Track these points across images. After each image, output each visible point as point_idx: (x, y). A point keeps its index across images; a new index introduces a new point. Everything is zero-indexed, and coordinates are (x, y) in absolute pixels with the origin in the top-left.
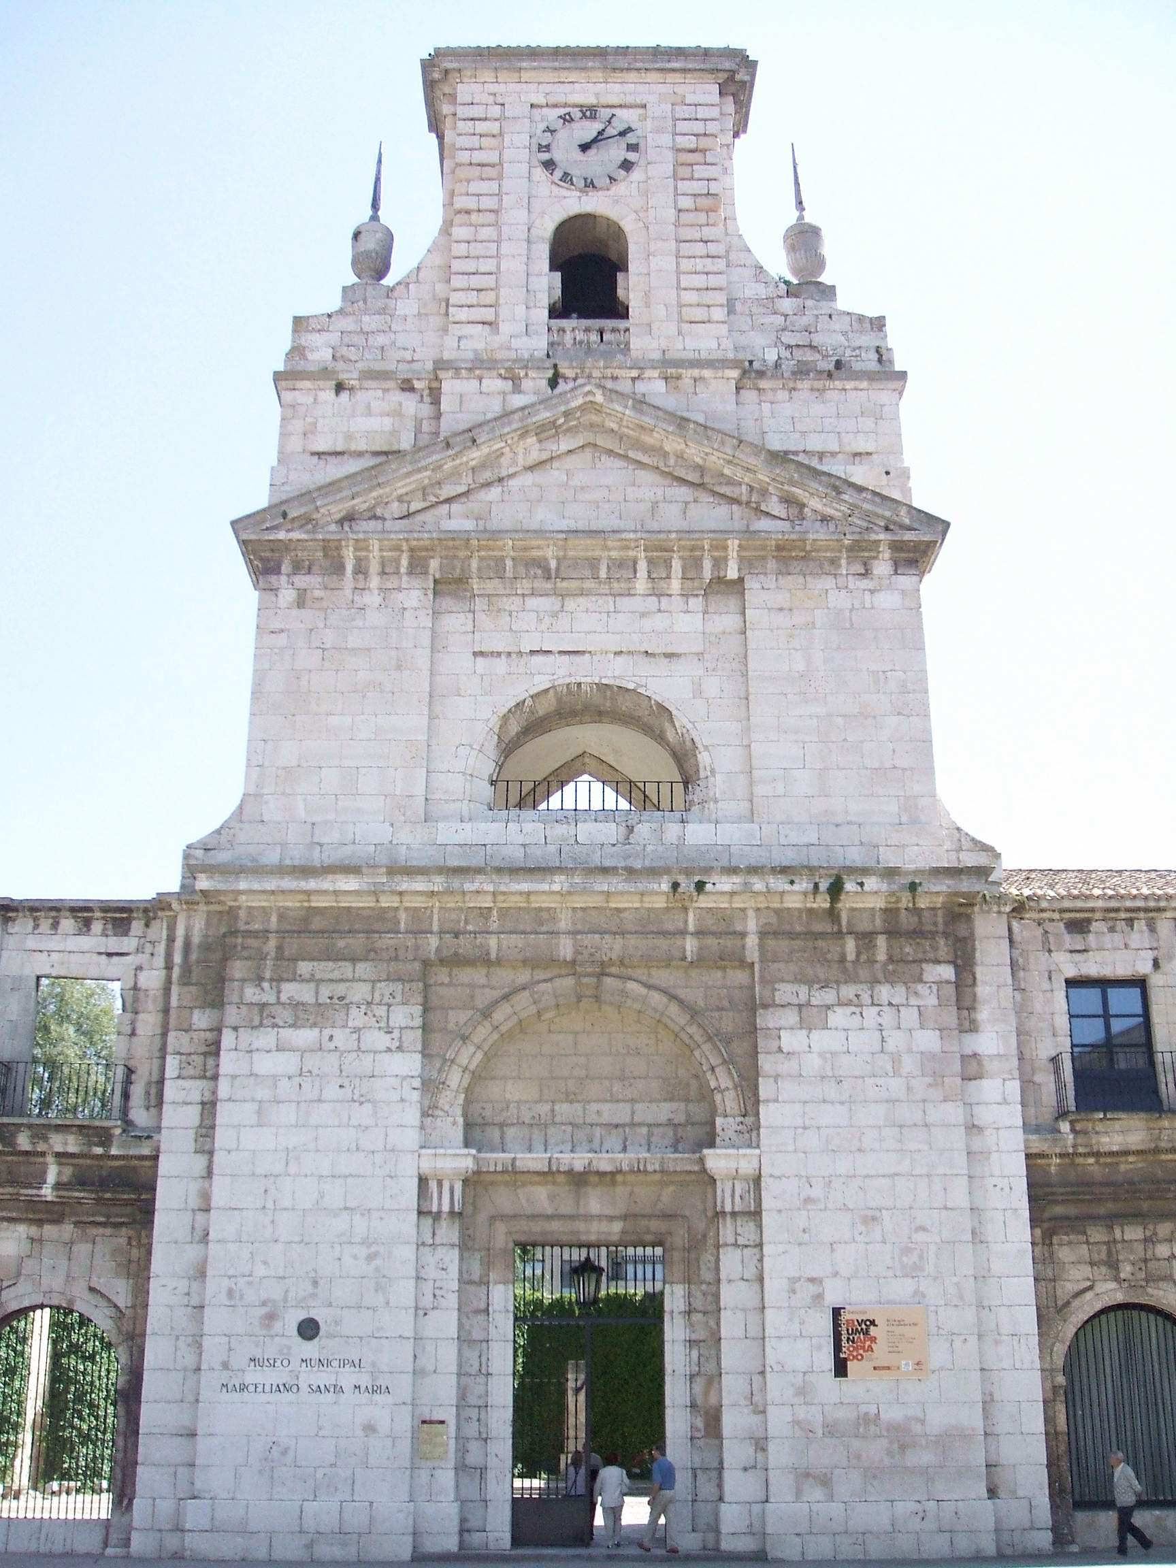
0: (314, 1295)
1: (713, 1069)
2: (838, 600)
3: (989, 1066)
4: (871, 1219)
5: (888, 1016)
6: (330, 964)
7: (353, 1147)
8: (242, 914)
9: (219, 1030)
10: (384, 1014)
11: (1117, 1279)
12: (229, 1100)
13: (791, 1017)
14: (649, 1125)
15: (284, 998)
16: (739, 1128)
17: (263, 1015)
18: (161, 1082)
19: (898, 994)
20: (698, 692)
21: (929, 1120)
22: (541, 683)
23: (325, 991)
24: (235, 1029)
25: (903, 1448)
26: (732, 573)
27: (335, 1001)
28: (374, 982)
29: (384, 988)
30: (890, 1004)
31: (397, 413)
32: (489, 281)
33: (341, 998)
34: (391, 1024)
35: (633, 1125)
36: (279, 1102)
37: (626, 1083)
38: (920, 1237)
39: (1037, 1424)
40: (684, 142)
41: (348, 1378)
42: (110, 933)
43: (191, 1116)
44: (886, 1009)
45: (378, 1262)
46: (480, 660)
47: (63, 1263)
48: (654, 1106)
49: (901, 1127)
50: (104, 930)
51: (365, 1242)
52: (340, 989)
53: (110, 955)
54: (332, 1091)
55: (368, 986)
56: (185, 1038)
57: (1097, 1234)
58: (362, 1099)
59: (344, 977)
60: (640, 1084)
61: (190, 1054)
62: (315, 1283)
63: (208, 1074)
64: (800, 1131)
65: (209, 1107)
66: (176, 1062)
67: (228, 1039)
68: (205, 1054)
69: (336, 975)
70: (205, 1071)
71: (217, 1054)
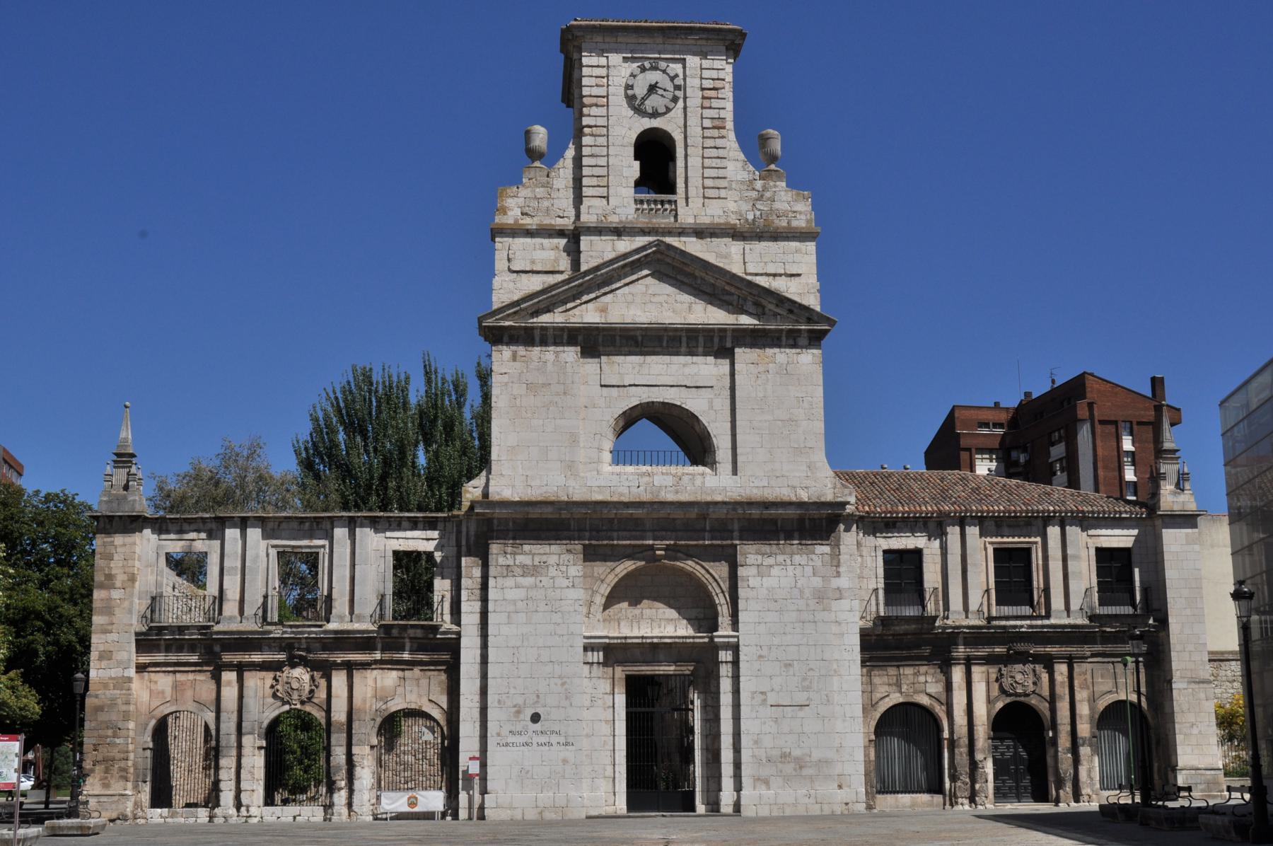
3: (845, 594)
4: (788, 665)
5: (799, 569)
8: (495, 522)
13: (753, 571)
20: (711, 407)
22: (635, 402)
23: (537, 559)
25: (801, 768)
26: (729, 345)
29: (566, 557)
32: (603, 172)
38: (811, 673)
39: (860, 756)
40: (707, 84)
41: (554, 739)
47: (415, 689)
51: (559, 677)
52: (544, 558)
54: (542, 607)
56: (470, 581)
57: (892, 671)
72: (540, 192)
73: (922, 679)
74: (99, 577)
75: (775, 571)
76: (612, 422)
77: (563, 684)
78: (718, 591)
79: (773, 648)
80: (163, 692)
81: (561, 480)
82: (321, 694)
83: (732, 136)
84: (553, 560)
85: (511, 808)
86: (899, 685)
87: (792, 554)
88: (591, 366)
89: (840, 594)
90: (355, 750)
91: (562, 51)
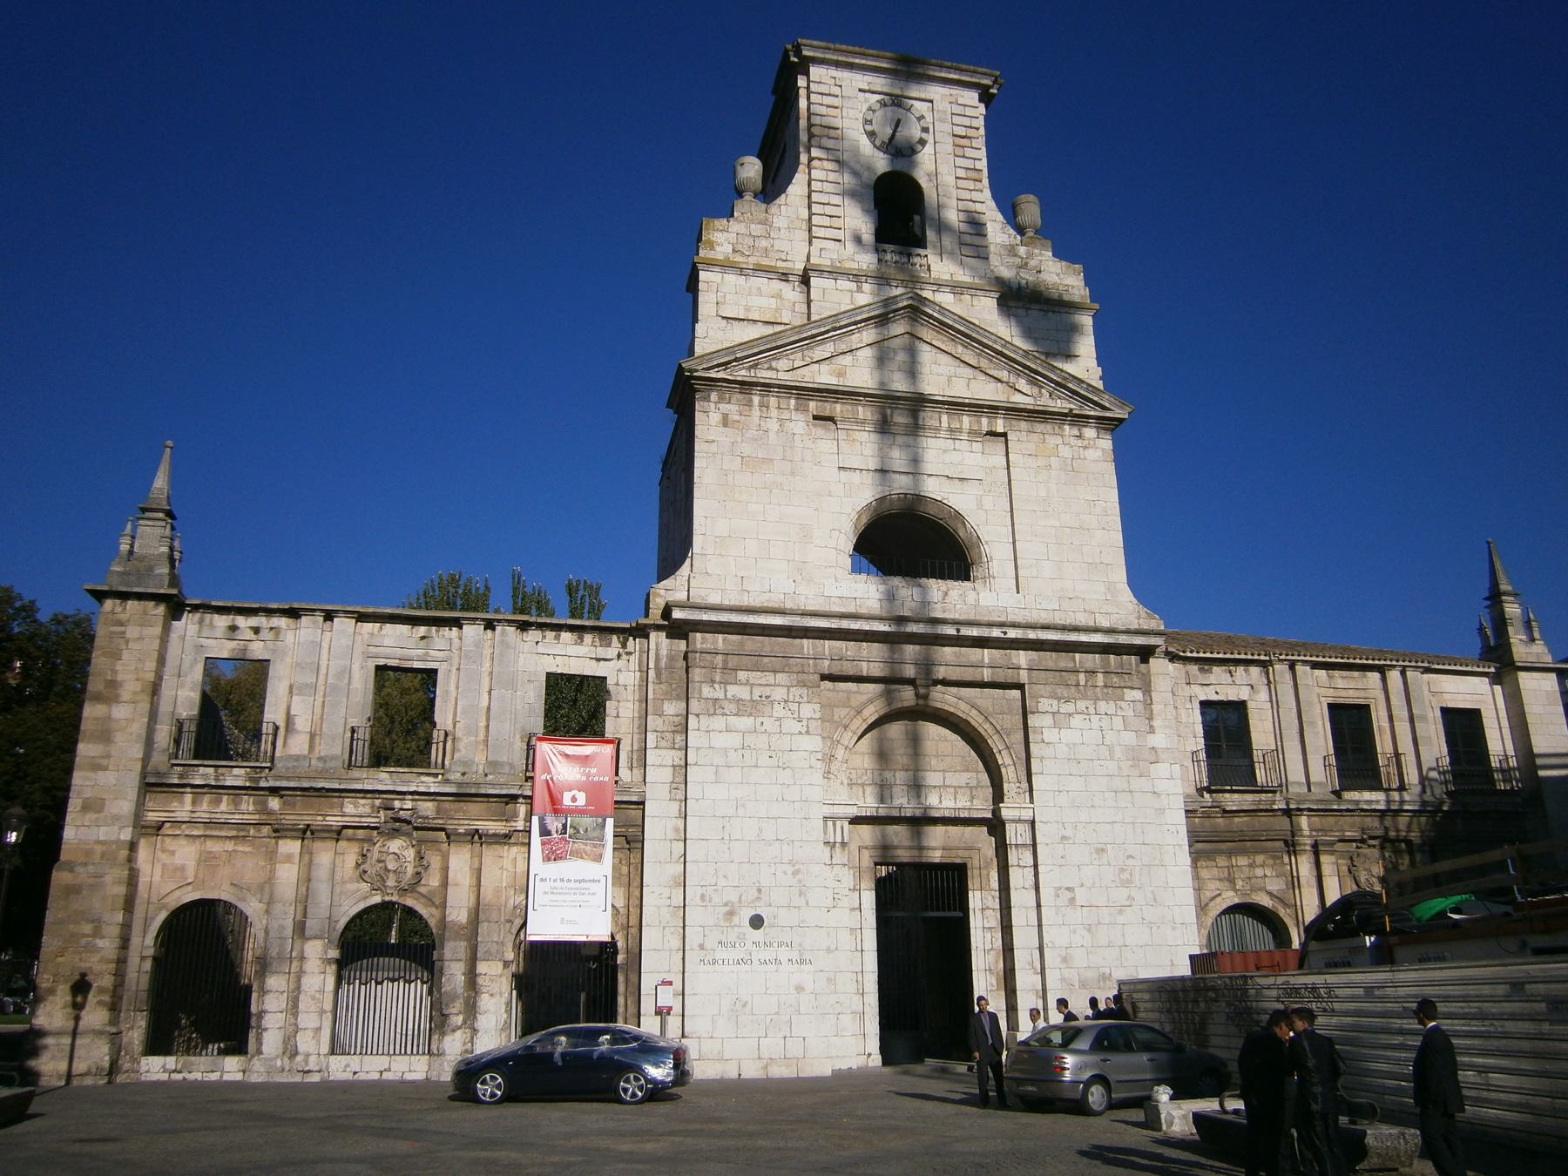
0: (758, 899)
2: (1065, 452)
3: (1163, 756)
5: (1106, 722)
11: (1236, 891)
13: (1047, 720)
17: (715, 707)
20: (980, 506)
23: (757, 692)
31: (779, 296)
35: (945, 786)
38: (1130, 862)
40: (960, 131)
45: (800, 876)
53: (598, 660)
54: (764, 760)
56: (659, 721)
57: (1222, 861)
60: (948, 759)
62: (759, 891)
67: (692, 721)
68: (674, 732)
69: (763, 681)
72: (757, 229)
73: (1259, 872)
74: (95, 685)
75: (1077, 721)
76: (854, 516)
77: (795, 873)
79: (1080, 826)
80: (182, 868)
81: (789, 587)
82: (433, 881)
83: (987, 193)
84: (779, 693)
85: (721, 1059)
86: (1231, 881)
89: (1155, 756)
90: (482, 967)
91: (774, 92)
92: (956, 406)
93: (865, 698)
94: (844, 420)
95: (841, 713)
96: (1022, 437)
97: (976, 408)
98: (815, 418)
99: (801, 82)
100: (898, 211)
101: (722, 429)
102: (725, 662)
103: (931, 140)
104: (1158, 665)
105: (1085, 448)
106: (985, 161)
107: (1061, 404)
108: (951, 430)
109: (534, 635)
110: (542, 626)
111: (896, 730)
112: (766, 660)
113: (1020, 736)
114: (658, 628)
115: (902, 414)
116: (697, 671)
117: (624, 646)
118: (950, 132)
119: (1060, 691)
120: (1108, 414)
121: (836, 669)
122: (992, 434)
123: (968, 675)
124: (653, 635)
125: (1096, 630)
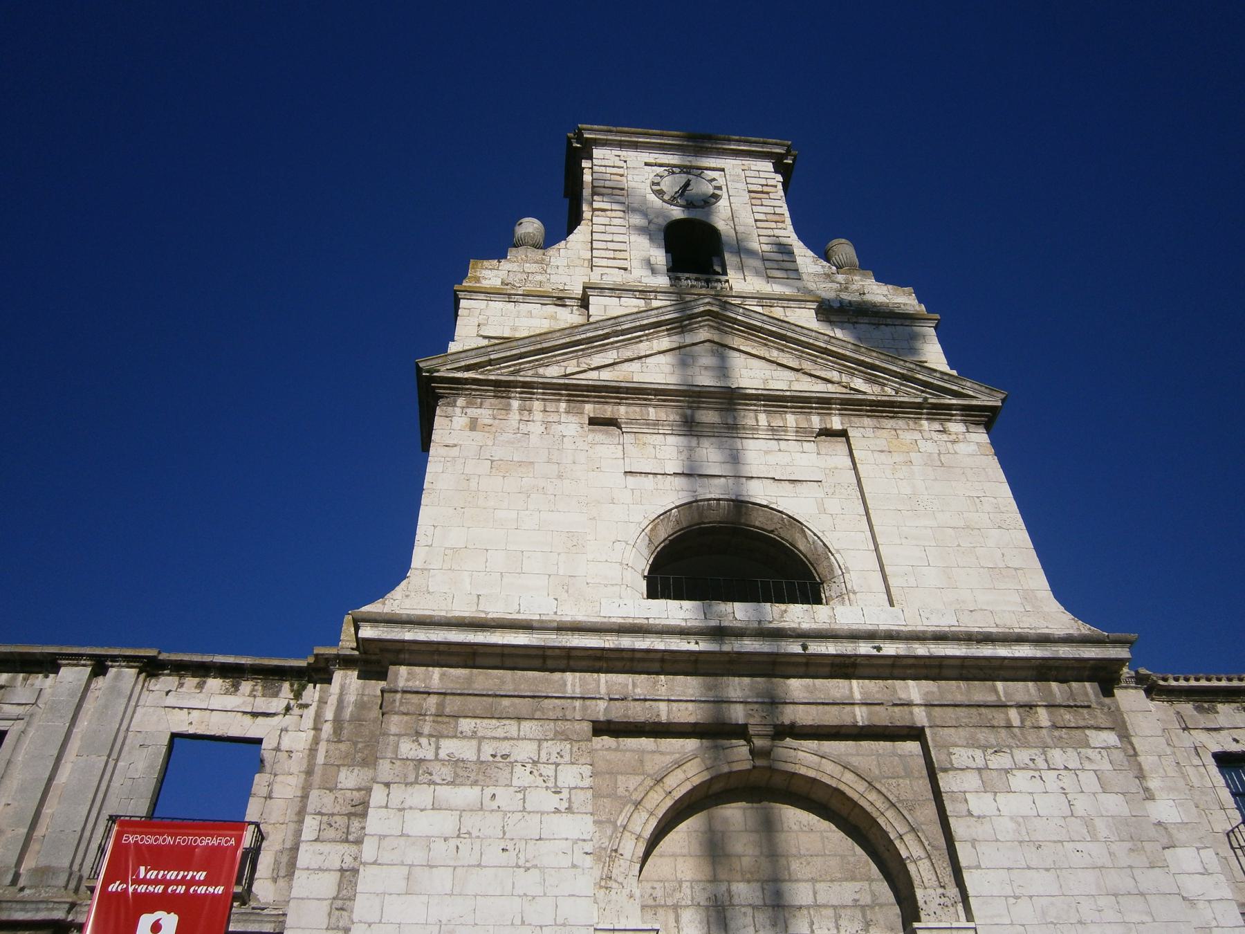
1: (901, 837)
3: (1181, 836)
5: (1068, 780)
6: (494, 721)
7: (518, 921)
9: (369, 790)
10: (551, 773)
12: (375, 863)
13: (970, 781)
14: (835, 907)
15: (443, 754)
16: (942, 900)
18: (295, 849)
19: (1070, 758)
21: (1143, 887)
23: (488, 749)
24: (387, 785)
27: (498, 759)
28: (540, 741)
29: (551, 748)
30: (1066, 768)
33: (504, 756)
34: (559, 784)
35: (817, 906)
36: (431, 867)
37: (803, 860)
42: (259, 694)
43: (327, 884)
44: (1063, 773)
46: (629, 478)
48: (836, 886)
49: (1116, 895)
50: (253, 690)
52: (505, 747)
53: (255, 715)
54: (493, 855)
55: (535, 745)
56: (328, 798)
58: (528, 865)
59: (508, 735)
60: (818, 861)
61: (333, 815)
63: (351, 838)
64: (1012, 900)
65: (348, 875)
66: (316, 823)
69: (500, 733)
70: (348, 833)
71: (364, 815)
75: (1019, 780)
78: (902, 829)
83: (791, 228)
87: (1045, 747)
88: (606, 446)
92: (775, 401)
93: (668, 759)
94: (631, 421)
95: (629, 784)
96: (864, 432)
97: (801, 403)
98: (593, 422)
99: (585, 164)
100: (693, 246)
101: (468, 433)
102: (441, 706)
103: (725, 196)
104: (1130, 699)
105: (954, 442)
106: (785, 206)
107: (910, 395)
108: (771, 429)
109: (167, 681)
110: (180, 669)
111: (734, 814)
112: (506, 702)
113: (931, 810)
114: (346, 662)
115: (710, 411)
116: (395, 718)
117: (298, 695)
118: (746, 193)
119: (983, 735)
120: (974, 402)
121: (618, 713)
122: (827, 433)
123: (831, 717)
124: (338, 676)
125: (1020, 639)
